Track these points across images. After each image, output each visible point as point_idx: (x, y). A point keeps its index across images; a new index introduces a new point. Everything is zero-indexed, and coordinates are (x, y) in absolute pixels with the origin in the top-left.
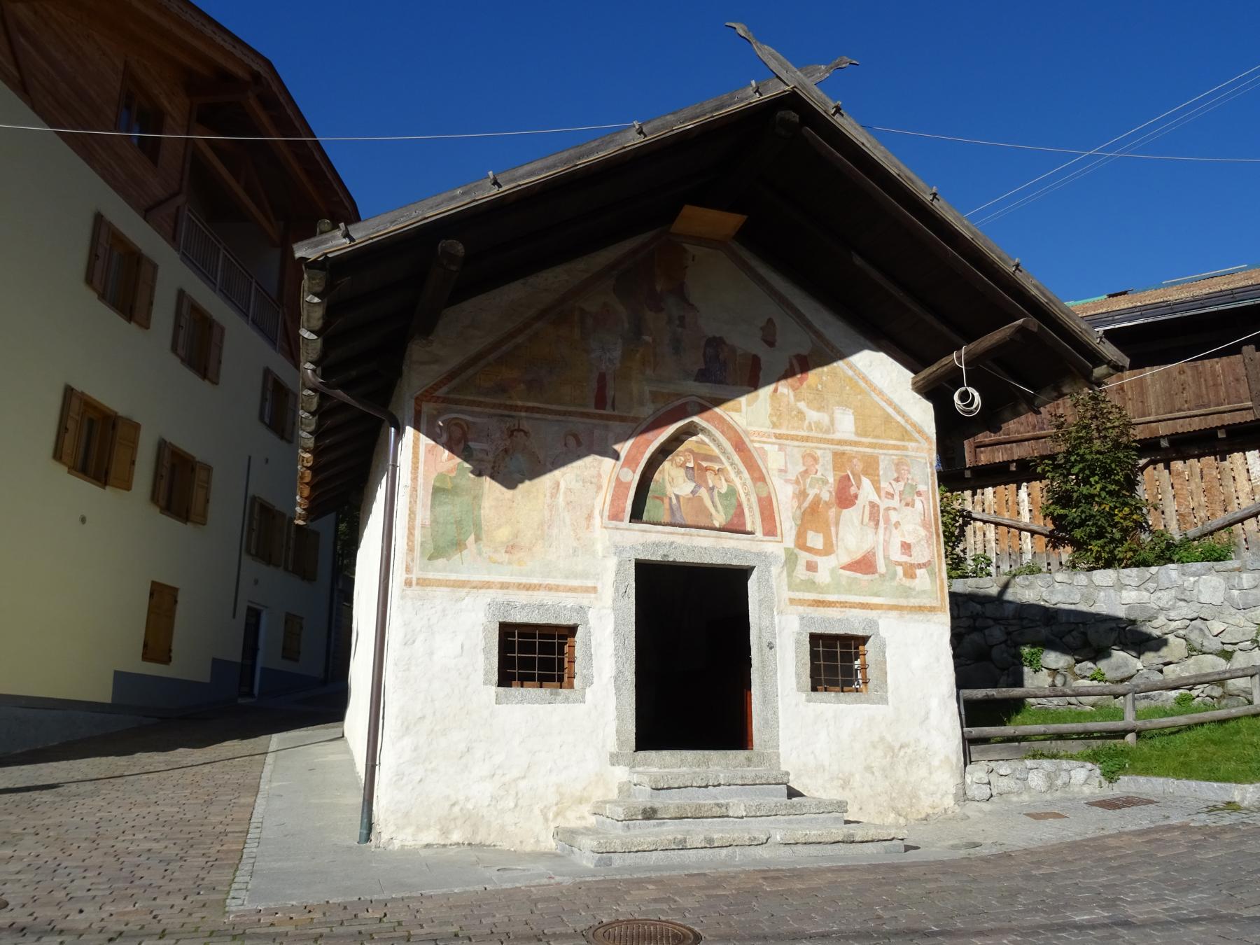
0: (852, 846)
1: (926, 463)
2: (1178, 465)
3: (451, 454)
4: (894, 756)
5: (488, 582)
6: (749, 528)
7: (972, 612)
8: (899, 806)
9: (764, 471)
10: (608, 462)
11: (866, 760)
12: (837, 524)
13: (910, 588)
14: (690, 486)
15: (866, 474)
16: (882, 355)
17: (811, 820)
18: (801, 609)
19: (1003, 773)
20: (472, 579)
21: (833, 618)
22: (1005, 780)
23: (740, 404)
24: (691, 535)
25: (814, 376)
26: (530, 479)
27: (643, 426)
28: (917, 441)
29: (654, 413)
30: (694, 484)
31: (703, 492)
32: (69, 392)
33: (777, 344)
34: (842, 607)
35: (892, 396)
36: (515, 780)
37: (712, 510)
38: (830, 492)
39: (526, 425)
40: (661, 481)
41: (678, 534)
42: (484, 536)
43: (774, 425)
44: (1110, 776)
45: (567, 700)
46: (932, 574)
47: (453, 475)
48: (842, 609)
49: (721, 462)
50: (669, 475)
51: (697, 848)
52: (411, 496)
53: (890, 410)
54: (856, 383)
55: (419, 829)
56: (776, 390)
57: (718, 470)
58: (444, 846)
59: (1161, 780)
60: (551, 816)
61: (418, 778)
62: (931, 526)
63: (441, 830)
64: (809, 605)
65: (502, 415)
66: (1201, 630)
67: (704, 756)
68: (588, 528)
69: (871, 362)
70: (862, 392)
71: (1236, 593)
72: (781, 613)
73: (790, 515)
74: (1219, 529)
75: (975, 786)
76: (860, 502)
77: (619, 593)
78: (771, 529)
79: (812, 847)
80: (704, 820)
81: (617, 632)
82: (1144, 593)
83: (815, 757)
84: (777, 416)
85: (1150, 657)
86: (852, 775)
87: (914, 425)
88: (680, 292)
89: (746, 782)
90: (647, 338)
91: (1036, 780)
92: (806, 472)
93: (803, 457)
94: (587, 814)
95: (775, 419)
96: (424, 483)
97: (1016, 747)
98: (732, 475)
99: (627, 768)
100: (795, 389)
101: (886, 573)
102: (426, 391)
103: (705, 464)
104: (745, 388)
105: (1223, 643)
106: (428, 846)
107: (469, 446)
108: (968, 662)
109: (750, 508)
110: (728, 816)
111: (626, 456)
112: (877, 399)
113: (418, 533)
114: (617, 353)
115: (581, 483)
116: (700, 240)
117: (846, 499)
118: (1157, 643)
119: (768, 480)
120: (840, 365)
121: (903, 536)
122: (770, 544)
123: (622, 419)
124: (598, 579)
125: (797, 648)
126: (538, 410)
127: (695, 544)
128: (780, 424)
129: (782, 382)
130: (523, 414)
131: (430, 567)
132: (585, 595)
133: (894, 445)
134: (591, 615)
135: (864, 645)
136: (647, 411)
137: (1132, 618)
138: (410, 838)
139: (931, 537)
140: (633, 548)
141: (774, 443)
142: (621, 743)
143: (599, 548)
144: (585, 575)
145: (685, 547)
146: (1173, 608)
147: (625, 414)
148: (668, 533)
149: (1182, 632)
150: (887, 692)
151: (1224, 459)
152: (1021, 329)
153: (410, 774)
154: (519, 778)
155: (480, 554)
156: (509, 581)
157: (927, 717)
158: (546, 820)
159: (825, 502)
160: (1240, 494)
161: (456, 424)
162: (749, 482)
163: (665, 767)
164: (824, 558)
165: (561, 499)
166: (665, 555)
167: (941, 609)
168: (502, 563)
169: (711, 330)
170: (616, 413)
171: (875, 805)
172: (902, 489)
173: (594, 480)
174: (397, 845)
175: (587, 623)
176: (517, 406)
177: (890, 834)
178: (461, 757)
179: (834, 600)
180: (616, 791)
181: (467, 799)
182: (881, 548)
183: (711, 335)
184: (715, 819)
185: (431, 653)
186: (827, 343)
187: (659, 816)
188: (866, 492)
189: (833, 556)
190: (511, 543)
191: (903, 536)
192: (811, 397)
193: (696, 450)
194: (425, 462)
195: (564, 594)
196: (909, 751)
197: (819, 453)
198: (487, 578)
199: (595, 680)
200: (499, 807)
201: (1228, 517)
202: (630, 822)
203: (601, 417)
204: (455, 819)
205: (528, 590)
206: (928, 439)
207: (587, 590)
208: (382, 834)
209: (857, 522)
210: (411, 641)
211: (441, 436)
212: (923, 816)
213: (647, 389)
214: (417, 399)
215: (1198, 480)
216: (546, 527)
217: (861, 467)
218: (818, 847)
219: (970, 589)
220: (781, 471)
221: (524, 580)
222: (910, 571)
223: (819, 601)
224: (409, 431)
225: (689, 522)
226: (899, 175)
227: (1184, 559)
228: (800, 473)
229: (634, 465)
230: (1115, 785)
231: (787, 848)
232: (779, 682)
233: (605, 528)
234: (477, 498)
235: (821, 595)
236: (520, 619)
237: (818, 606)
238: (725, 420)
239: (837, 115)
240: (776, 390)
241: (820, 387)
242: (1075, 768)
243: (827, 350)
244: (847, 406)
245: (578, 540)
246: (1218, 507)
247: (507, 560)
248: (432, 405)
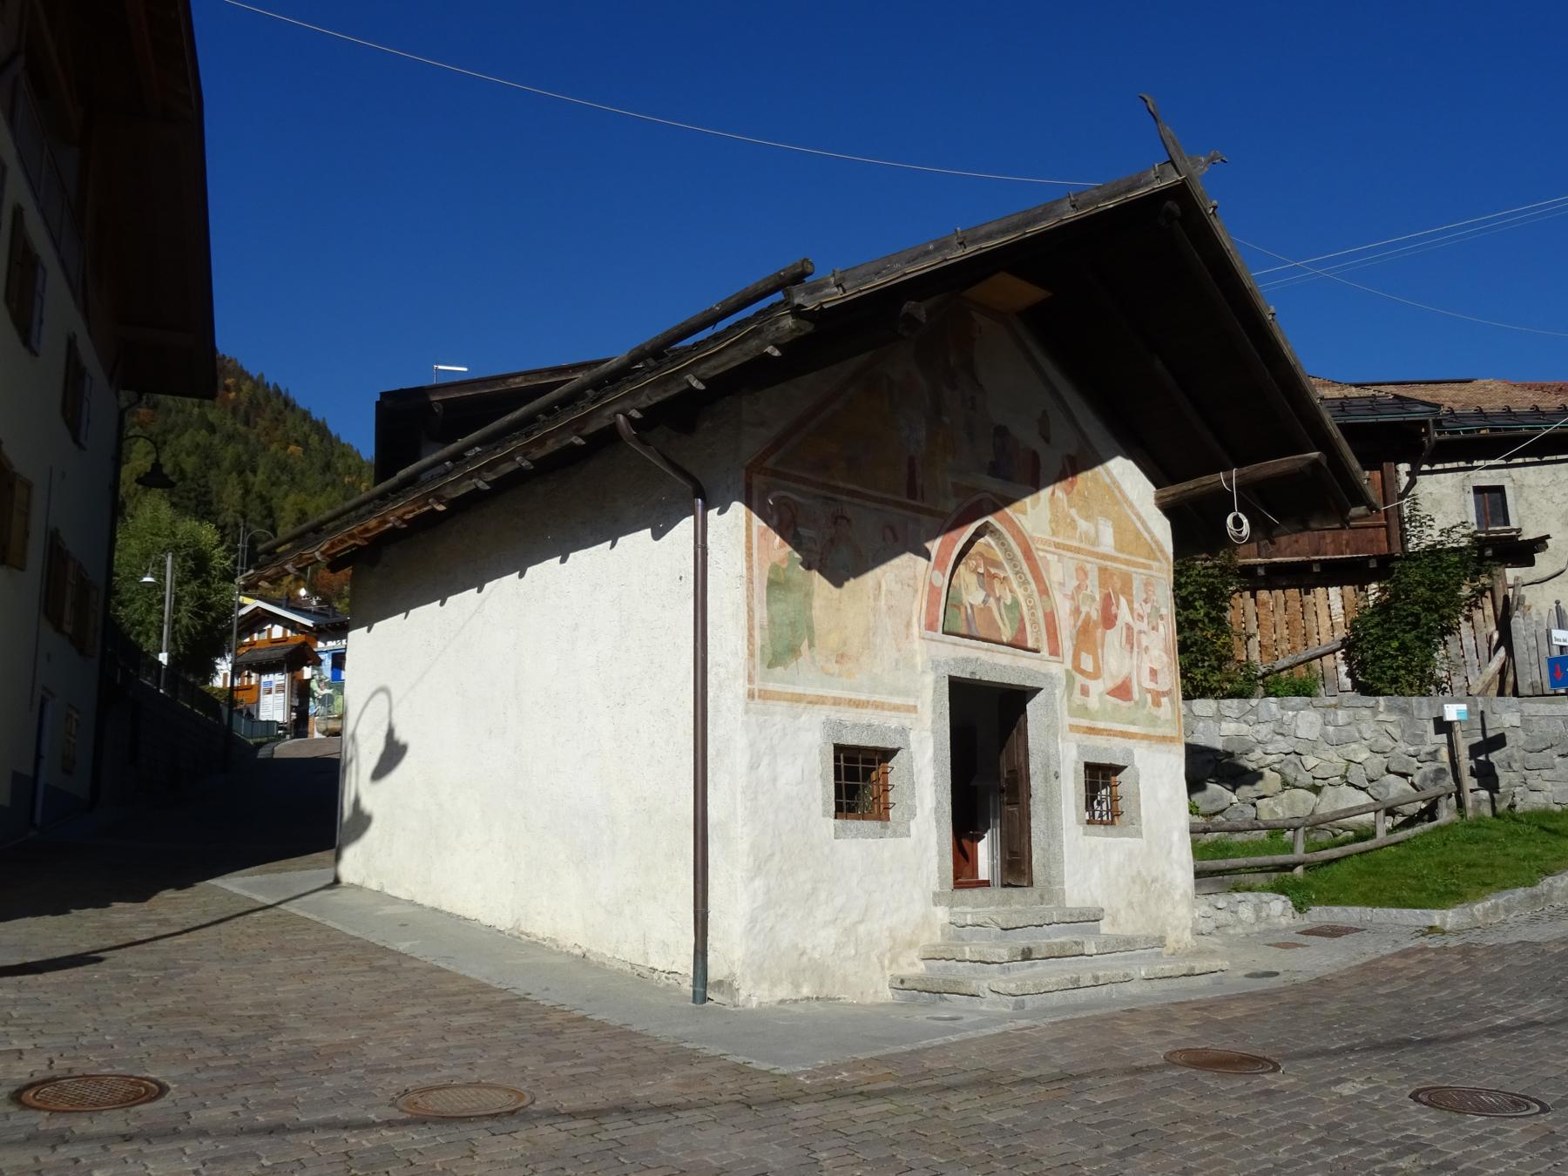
2: (1263, 595)
5: (822, 697)
6: (1030, 644)
10: (922, 561)
17: (1140, 956)
20: (807, 692)
26: (855, 576)
41: (983, 649)
42: (816, 642)
43: (1054, 533)
44: (1300, 908)
52: (748, 590)
55: (773, 984)
56: (1053, 494)
59: (1358, 909)
60: (886, 962)
63: (792, 983)
65: (826, 498)
66: (1296, 764)
68: (907, 637)
70: (1117, 503)
71: (1331, 729)
74: (1299, 664)
75: (1202, 920)
76: (1120, 623)
78: (1055, 652)
82: (1244, 725)
84: (1060, 522)
85: (1246, 791)
87: (1157, 542)
91: (1246, 912)
92: (1079, 587)
93: (1077, 570)
94: (916, 960)
99: (947, 908)
100: (1068, 493)
103: (993, 571)
105: (1314, 778)
106: (782, 1002)
107: (798, 533)
109: (1034, 623)
112: (1129, 512)
113: (757, 633)
118: (1254, 777)
120: (1099, 469)
121: (1151, 661)
123: (931, 513)
124: (917, 698)
127: (996, 661)
129: (1058, 485)
130: (844, 498)
132: (908, 714)
134: (912, 736)
135: (1116, 775)
136: (951, 506)
137: (1229, 750)
138: (766, 993)
139: (1171, 665)
140: (946, 663)
141: (1054, 553)
142: (942, 882)
143: (919, 660)
144: (907, 693)
145: (989, 664)
146: (1271, 741)
149: (1277, 766)
151: (1307, 593)
152: (1315, 462)
155: (813, 662)
157: (1169, 852)
158: (883, 968)
159: (1094, 621)
160: (1321, 630)
161: (785, 504)
166: (973, 673)
168: (832, 675)
170: (925, 505)
173: (911, 582)
174: (754, 1004)
175: (908, 746)
180: (939, 933)
181: (814, 948)
185: (774, 780)
187: (1034, 956)
188: (1123, 614)
189: (1100, 680)
190: (840, 652)
192: (1081, 503)
195: (887, 713)
196: (1158, 885)
197: (1088, 566)
198: (821, 692)
199: (918, 811)
200: (842, 955)
201: (1311, 653)
205: (857, 707)
208: (741, 991)
214: (747, 469)
215: (1282, 611)
216: (871, 634)
218: (1169, 980)
220: (1060, 584)
221: (853, 696)
227: (1280, 693)
230: (1305, 915)
233: (923, 638)
234: (808, 595)
240: (1053, 494)
242: (1272, 901)
246: (1299, 641)
247: (837, 671)
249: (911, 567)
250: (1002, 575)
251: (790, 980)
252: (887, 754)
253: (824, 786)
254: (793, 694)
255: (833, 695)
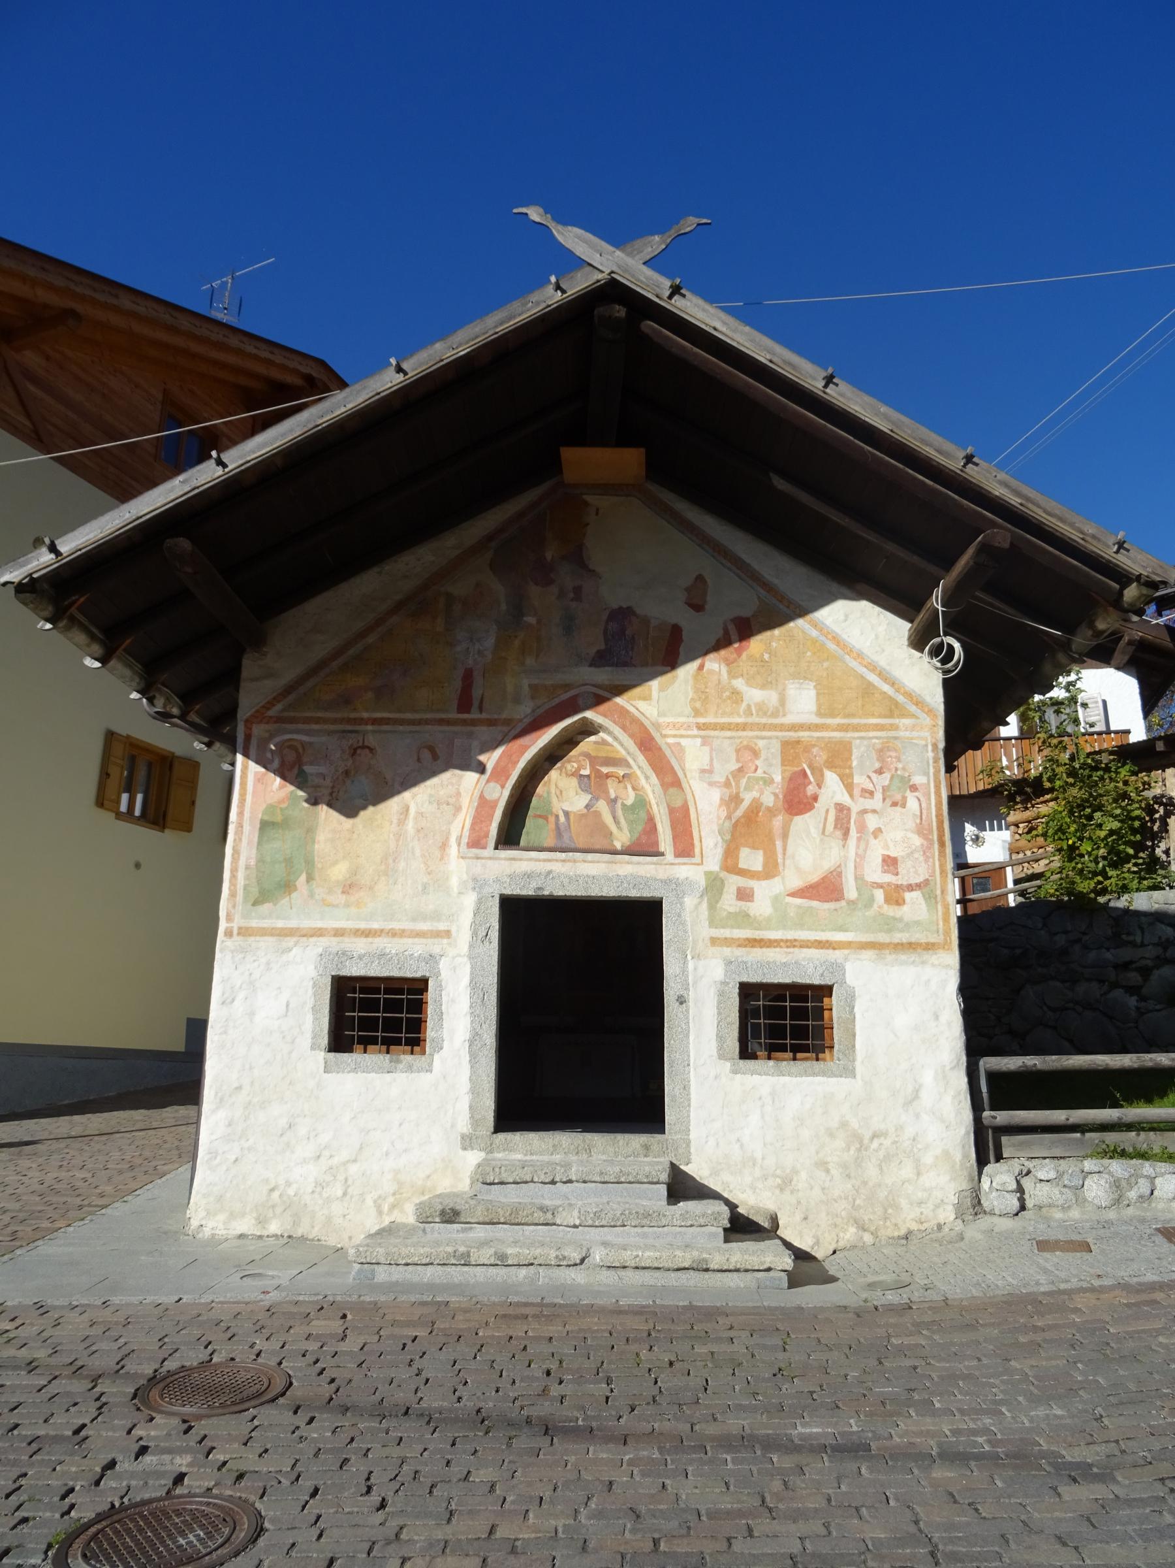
0: (707, 1275)
1: (926, 745)
3: (283, 782)
4: (862, 1147)
7: (1160, 938)
8: (866, 1218)
9: (680, 774)
10: (471, 777)
11: (817, 1153)
12: (785, 836)
13: (894, 919)
14: (585, 799)
15: (831, 765)
16: (865, 604)
18: (727, 951)
19: (1043, 1178)
20: (301, 926)
21: (775, 962)
22: (1046, 1187)
23: (650, 690)
24: (575, 861)
25: (757, 644)
26: (374, 804)
27: (518, 729)
28: (913, 716)
29: (533, 711)
30: (590, 796)
31: (602, 806)
32: (110, 736)
33: (707, 607)
34: (788, 947)
35: (875, 658)
36: (345, 1164)
37: (613, 828)
38: (776, 795)
39: (371, 740)
40: (545, 795)
42: (317, 875)
43: (697, 713)
45: (410, 1069)
46: (930, 898)
47: (284, 805)
48: (791, 950)
49: (628, 766)
50: (556, 786)
51: (484, 1265)
53: (873, 678)
54: (823, 645)
55: (232, 1216)
56: (701, 667)
57: (623, 776)
58: (260, 1237)
60: (386, 1208)
61: (233, 1158)
62: (931, 831)
63: (257, 1219)
64: (739, 946)
65: (344, 731)
67: (584, 1141)
69: (847, 616)
72: (697, 957)
73: (715, 828)
75: (994, 1194)
77: (479, 937)
78: (685, 848)
79: (647, 1273)
80: (526, 1227)
81: (473, 985)
83: (742, 1146)
84: (702, 699)
86: (795, 1171)
87: (909, 695)
88: (577, 558)
89: (607, 1179)
90: (531, 620)
91: (1096, 1190)
92: (741, 770)
93: (738, 751)
95: (698, 705)
96: (250, 817)
97: (1076, 1139)
98: (643, 781)
100: (728, 663)
101: (858, 899)
102: (257, 711)
103: (605, 770)
104: (660, 668)
106: (241, 1236)
108: (1158, 1007)
110: (555, 1224)
111: (494, 768)
112: (853, 664)
114: (490, 642)
115: (435, 805)
116: (606, 489)
117: (799, 802)
119: (685, 785)
120: (799, 625)
122: (683, 867)
123: (491, 723)
125: (719, 1003)
126: (386, 721)
128: (706, 711)
129: (712, 656)
130: (370, 728)
131: (253, 914)
133: (877, 725)
134: (443, 965)
136: (524, 710)
138: (221, 1226)
140: (497, 880)
141: (695, 736)
142: (475, 1122)
143: (454, 882)
147: (496, 716)
148: (545, 860)
150: (854, 1061)
153: (224, 1153)
154: (348, 1161)
155: (311, 895)
156: (345, 926)
159: (769, 809)
161: (289, 747)
162: (658, 788)
163: (531, 1154)
164: (764, 883)
165: (410, 826)
166: (539, 889)
167: (945, 946)
169: (615, 598)
170: (484, 716)
171: (828, 1214)
172: (887, 783)
173: (452, 801)
174: (207, 1232)
175: (438, 974)
176: (362, 719)
177: (762, 1263)
178: (282, 1135)
179: (777, 938)
181: (288, 1184)
182: (851, 865)
183: (615, 606)
184: (540, 1227)
185: (252, 1014)
186: (782, 598)
187: (462, 1220)
188: (832, 789)
189: (776, 879)
190: (349, 883)
191: (887, 847)
193: (593, 754)
194: (254, 792)
195: (410, 940)
196: (887, 1142)
197: (761, 744)
198: (319, 924)
200: (325, 1195)
202: (427, 1225)
203: (465, 722)
204: (273, 1207)
205: (367, 936)
206: (931, 712)
207: (438, 934)
209: (815, 832)
210: (229, 1001)
211: (273, 761)
212: (903, 1232)
213: (525, 683)
217: (825, 757)
218: (657, 1274)
219: (1156, 906)
220: (703, 771)
221: (363, 925)
222: (895, 895)
223: (755, 940)
224: (239, 758)
225: (581, 846)
226: (771, 361)
228: (732, 773)
229: (503, 778)
231: (612, 1272)
232: (691, 1046)
233: (462, 858)
234: (310, 831)
235: (758, 932)
236: (356, 971)
237: (752, 947)
238: (627, 711)
239: (676, 297)
240: (701, 667)
241: (766, 656)
242: (1162, 1175)
243: (781, 606)
244: (805, 678)
245: (429, 874)
248: (263, 727)
249: (452, 784)
250: (621, 773)
251: (255, 1215)
252: (827, 990)
253: (315, 1019)
254: (282, 929)
255: (334, 926)
